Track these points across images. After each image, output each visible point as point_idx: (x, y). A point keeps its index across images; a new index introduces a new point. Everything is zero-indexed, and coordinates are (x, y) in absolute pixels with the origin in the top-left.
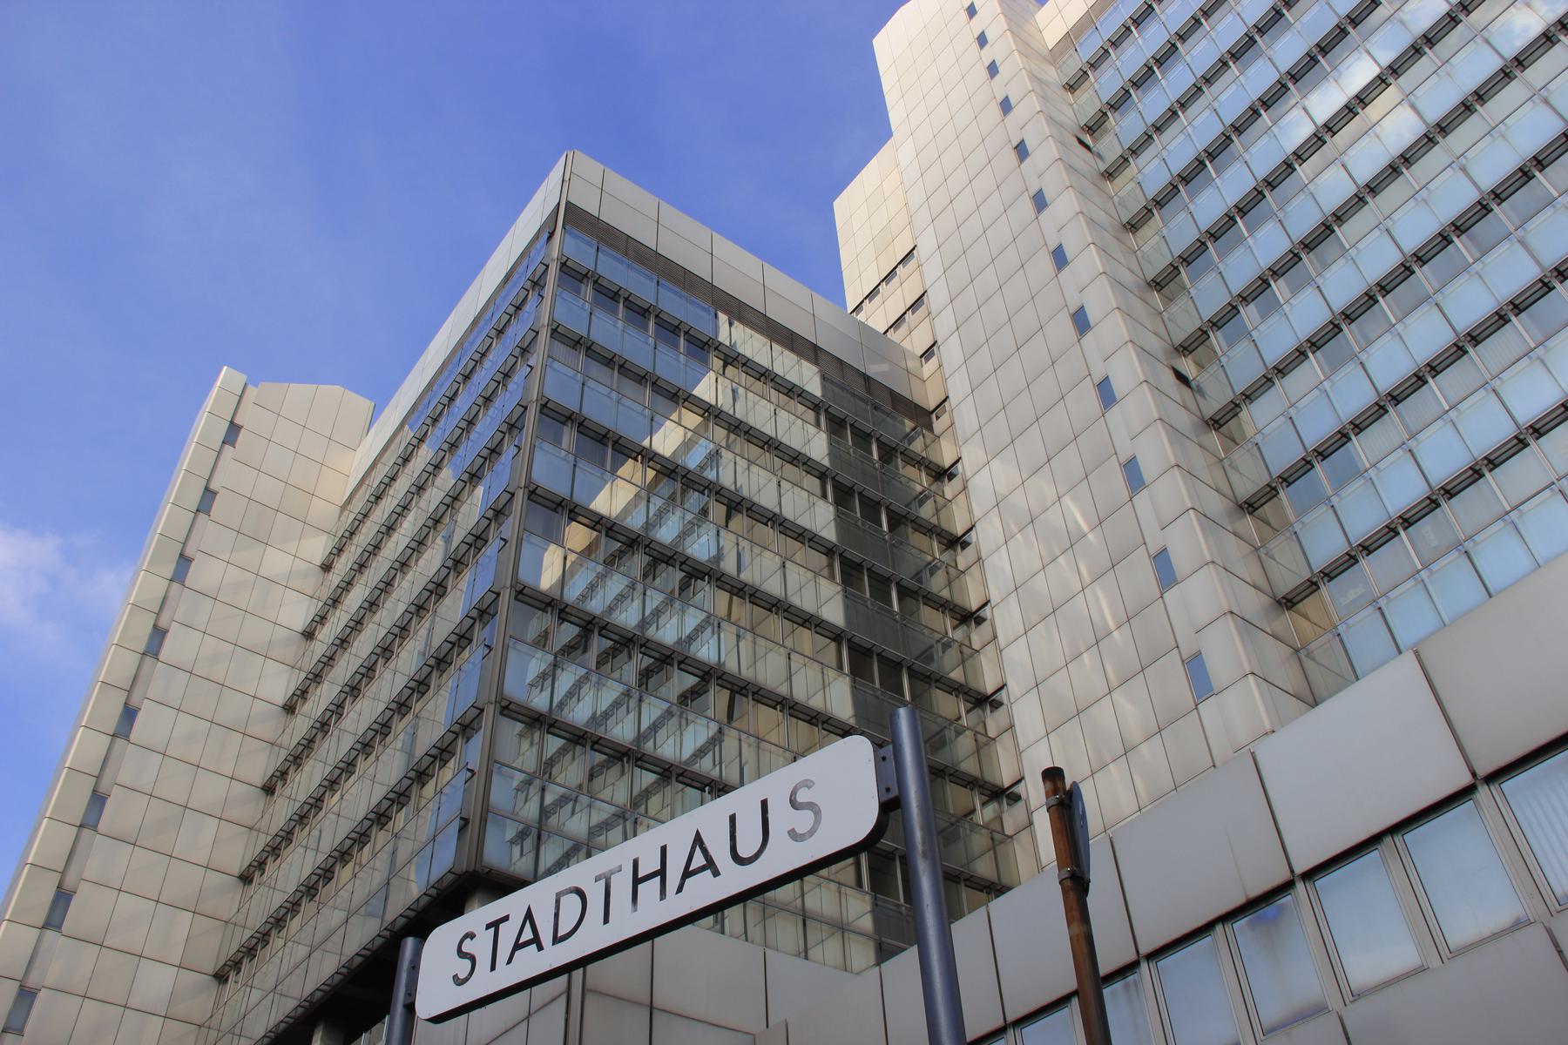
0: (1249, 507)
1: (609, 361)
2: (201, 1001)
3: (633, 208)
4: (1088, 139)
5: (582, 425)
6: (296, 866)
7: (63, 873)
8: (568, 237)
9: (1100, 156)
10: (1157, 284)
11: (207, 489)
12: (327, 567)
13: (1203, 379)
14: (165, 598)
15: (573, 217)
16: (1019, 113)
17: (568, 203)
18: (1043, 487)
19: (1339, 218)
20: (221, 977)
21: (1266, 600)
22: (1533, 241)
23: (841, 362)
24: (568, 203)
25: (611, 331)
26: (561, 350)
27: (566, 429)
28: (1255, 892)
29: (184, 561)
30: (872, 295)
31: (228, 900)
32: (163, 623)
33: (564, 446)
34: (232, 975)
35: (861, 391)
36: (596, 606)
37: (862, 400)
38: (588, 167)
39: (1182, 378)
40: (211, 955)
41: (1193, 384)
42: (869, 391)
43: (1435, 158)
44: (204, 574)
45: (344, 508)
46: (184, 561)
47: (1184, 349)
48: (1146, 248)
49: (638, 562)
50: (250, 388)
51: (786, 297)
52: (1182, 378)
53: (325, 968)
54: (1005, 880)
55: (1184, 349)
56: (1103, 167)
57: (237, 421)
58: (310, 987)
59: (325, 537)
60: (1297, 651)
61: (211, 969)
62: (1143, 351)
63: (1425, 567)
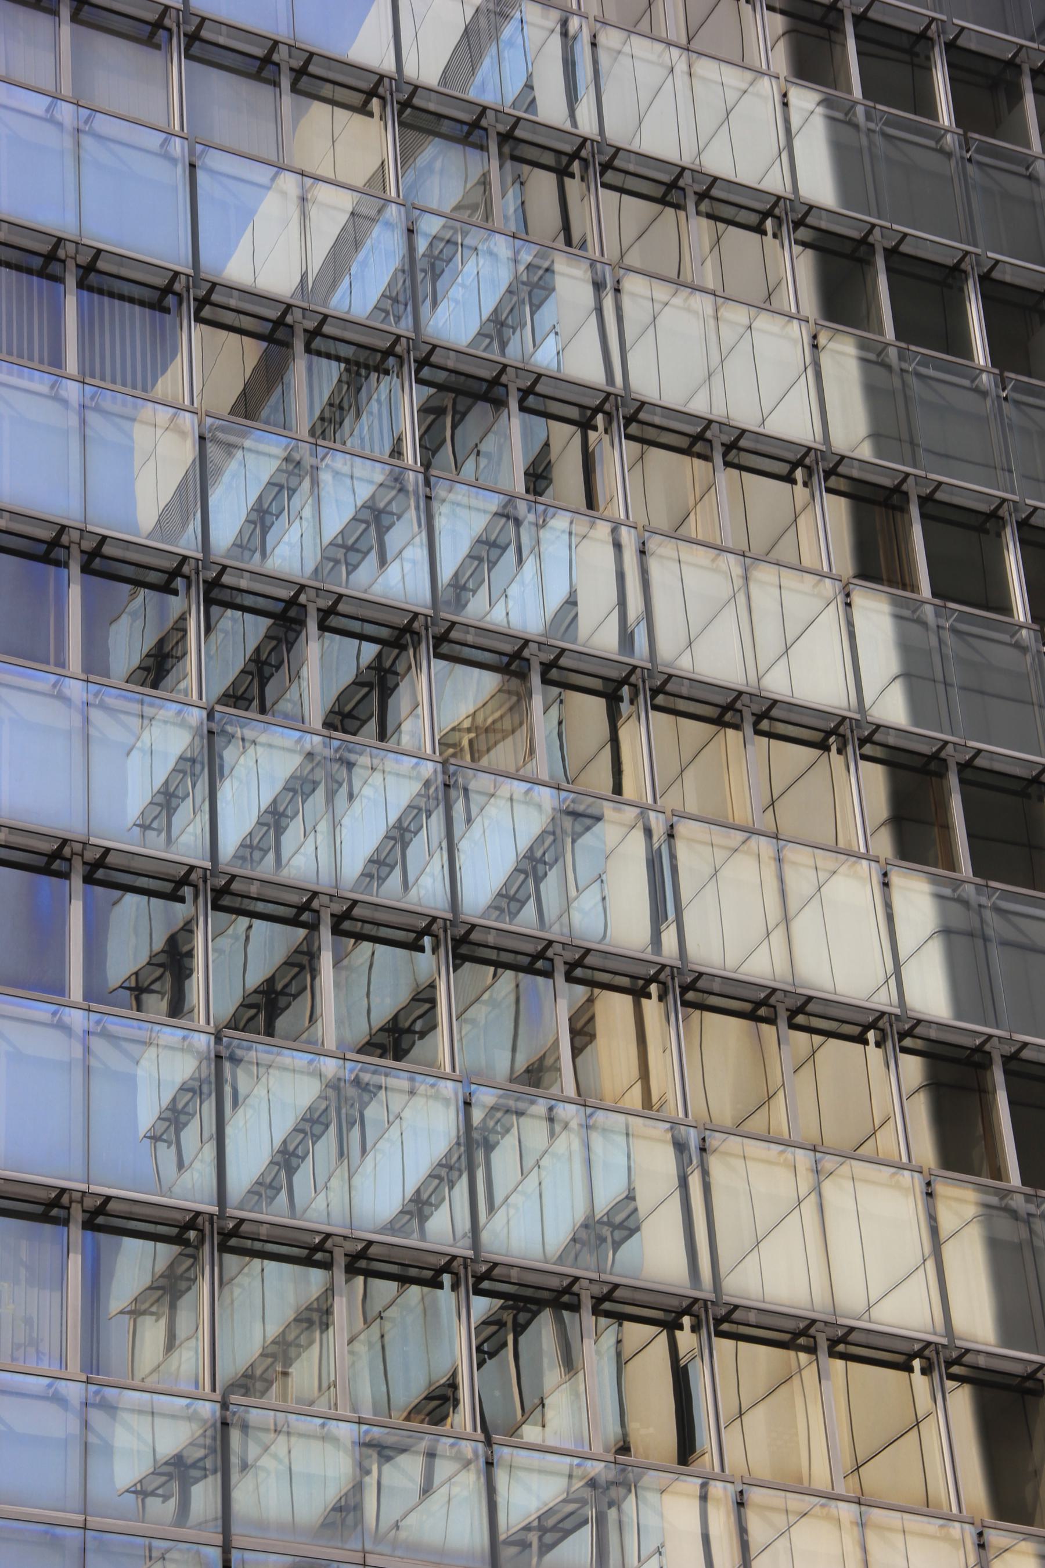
49: (397, 406)
59: (883, 829)
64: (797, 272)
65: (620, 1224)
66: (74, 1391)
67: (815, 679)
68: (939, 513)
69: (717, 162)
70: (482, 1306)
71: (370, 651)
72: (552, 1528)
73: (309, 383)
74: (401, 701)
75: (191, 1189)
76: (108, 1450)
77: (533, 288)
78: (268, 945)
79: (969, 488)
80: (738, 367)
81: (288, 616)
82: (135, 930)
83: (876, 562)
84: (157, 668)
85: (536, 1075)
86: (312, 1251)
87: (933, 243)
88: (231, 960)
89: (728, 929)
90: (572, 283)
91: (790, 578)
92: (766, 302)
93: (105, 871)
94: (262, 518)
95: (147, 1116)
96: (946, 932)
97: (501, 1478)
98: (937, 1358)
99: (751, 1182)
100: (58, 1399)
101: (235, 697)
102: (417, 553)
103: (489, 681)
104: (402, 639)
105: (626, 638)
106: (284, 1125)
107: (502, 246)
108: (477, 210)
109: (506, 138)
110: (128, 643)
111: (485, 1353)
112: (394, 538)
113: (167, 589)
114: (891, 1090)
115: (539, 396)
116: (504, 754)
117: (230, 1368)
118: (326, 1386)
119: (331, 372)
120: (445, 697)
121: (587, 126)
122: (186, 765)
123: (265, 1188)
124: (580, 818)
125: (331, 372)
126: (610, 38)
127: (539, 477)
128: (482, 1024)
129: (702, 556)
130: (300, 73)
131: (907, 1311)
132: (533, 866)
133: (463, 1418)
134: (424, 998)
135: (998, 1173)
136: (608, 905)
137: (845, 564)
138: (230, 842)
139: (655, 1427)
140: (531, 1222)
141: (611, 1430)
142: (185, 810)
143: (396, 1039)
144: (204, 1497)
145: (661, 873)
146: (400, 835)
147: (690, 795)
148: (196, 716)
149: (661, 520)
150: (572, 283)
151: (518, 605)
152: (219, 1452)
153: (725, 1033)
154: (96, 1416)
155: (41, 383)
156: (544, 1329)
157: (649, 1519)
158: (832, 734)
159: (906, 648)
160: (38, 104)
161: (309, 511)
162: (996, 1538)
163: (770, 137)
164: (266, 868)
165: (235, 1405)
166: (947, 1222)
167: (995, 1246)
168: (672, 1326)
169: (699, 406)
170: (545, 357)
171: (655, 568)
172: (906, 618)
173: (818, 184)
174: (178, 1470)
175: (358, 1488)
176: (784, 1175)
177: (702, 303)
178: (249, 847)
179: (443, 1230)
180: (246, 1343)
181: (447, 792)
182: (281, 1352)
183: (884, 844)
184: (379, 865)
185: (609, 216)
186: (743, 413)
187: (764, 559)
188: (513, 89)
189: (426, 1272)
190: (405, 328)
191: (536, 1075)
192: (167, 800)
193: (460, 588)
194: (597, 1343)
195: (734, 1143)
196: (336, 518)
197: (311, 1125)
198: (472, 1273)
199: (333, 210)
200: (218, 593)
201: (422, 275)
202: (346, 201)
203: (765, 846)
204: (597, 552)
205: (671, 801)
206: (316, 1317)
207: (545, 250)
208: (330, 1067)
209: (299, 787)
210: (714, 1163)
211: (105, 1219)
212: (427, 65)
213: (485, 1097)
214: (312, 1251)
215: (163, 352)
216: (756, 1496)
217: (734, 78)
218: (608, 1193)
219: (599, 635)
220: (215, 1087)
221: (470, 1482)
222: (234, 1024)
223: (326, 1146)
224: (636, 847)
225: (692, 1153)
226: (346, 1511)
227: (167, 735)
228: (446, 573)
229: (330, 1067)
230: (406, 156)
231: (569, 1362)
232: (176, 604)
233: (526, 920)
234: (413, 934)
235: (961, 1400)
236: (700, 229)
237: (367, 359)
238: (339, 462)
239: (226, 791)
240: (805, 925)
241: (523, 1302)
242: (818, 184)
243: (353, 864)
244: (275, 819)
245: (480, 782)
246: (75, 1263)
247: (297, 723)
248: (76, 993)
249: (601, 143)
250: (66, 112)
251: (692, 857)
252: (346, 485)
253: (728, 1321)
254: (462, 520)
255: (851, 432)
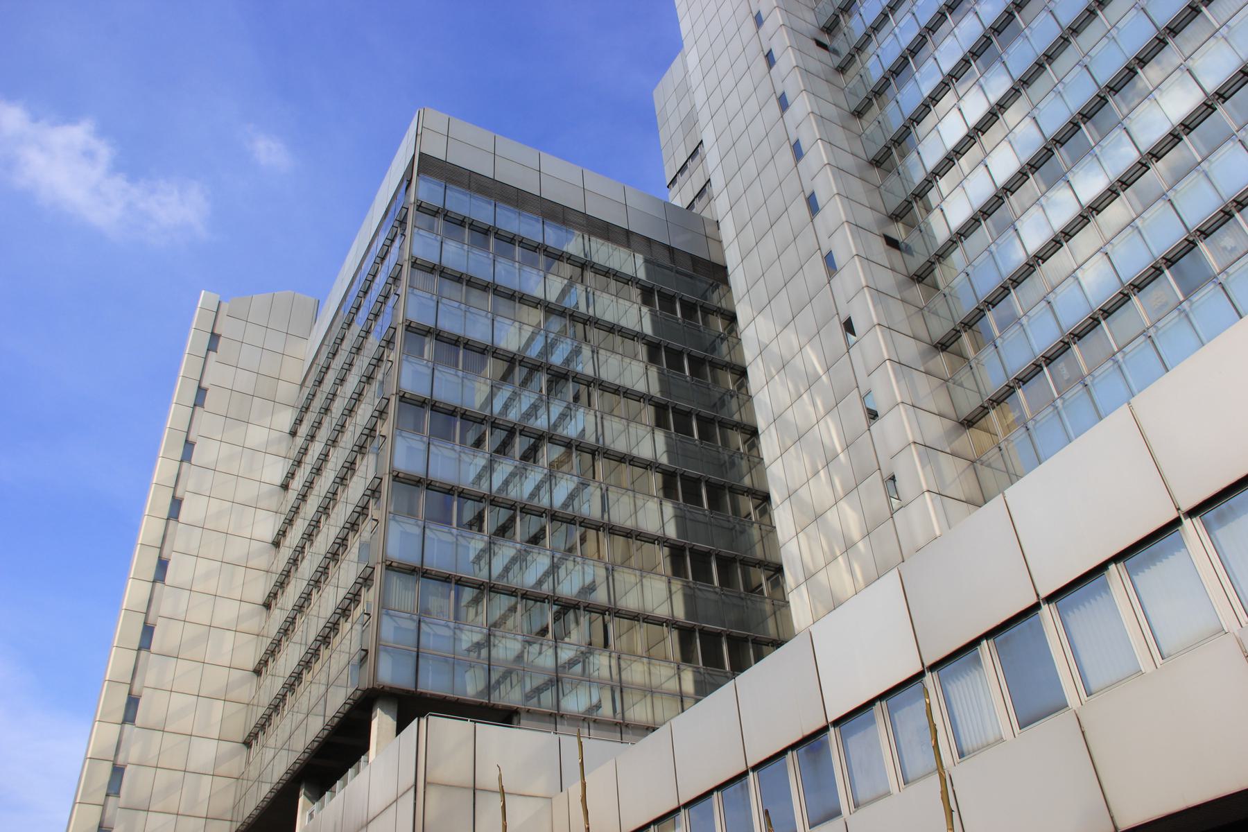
0: (942, 346)
1: (458, 278)
2: (235, 765)
3: (473, 147)
4: (825, 39)
5: (438, 335)
6: (290, 657)
7: (131, 684)
8: (421, 182)
9: (835, 52)
10: (877, 162)
11: (199, 387)
12: (293, 433)
13: (914, 240)
14: (178, 475)
15: (427, 165)
16: (769, 26)
17: (421, 154)
18: (791, 337)
19: (1049, 57)
20: (247, 744)
21: (949, 424)
22: (1134, 129)
23: (648, 240)
24: (421, 154)
25: (456, 254)
26: (420, 275)
27: (427, 339)
28: (807, 732)
29: (189, 445)
30: (683, 169)
31: (246, 690)
32: (179, 494)
33: (426, 357)
34: (254, 742)
35: (667, 262)
36: (513, 415)
37: (667, 268)
38: (436, 119)
39: (892, 243)
40: (240, 729)
41: (903, 246)
42: (673, 260)
43: (1066, 60)
44: (204, 453)
45: (302, 385)
46: (189, 445)
47: (896, 217)
48: (867, 132)
49: (542, 380)
50: (223, 304)
51: (601, 195)
52: (892, 243)
53: (316, 727)
54: (782, 637)
55: (896, 217)
56: (837, 61)
57: (216, 331)
58: (311, 737)
59: (291, 410)
60: (973, 462)
61: (241, 739)
62: (856, 227)
63: (1120, 350)
64: (642, 350)
65: (591, 588)
66: (452, 625)
67: (644, 450)
68: (676, 411)
69: (623, 323)
70: (555, 608)
71: (532, 441)
72: (572, 663)
73: (519, 373)
74: (540, 454)
75: (482, 576)
76: (460, 640)
77: (577, 352)
78: (504, 515)
79: (684, 405)
80: (627, 373)
81: (511, 431)
82: (470, 510)
83: (661, 423)
84: (478, 443)
85: (571, 550)
86: (512, 593)
87: (676, 345)
88: (492, 519)
89: (621, 514)
90: (586, 351)
91: (639, 426)
92: (635, 357)
93: (463, 495)
94: (506, 407)
95: (472, 556)
96: (676, 516)
97: (559, 651)
98: (671, 623)
99: (625, 578)
100: (448, 626)
101: (497, 451)
102: (545, 416)
103: (562, 449)
104: (540, 438)
105: (597, 440)
106: (506, 561)
107: (569, 341)
108: (563, 333)
109: (571, 315)
110: (471, 437)
111: (556, 619)
112: (539, 413)
113: (481, 423)
114: (661, 556)
115: (577, 378)
116: (565, 468)
117: (491, 621)
118: (515, 627)
119: (525, 371)
120: (549, 453)
121: (591, 313)
122: (484, 468)
123: (501, 576)
124: (584, 485)
125: (525, 371)
126: (598, 293)
127: (576, 398)
128: (555, 537)
129: (617, 419)
130: (521, 298)
131: (662, 611)
132: (572, 497)
133: (550, 635)
134: (543, 530)
135: (687, 577)
136: (590, 507)
137: (653, 423)
138: (495, 488)
139: (598, 639)
140: (569, 587)
141: (587, 639)
142: (484, 480)
143: (536, 539)
144: (484, 652)
145: (604, 499)
146: (538, 488)
147: (612, 480)
148: (487, 456)
149: (607, 410)
150: (586, 351)
151: (571, 430)
152: (488, 642)
153: (620, 540)
154: (458, 632)
155: (452, 371)
156: (571, 615)
157: (596, 662)
158: (648, 465)
159: (668, 444)
160: (456, 304)
161: (517, 404)
162: (682, 667)
163: (636, 318)
164: (504, 495)
165: (494, 627)
166: (674, 589)
167: (685, 596)
168: (603, 614)
169: (617, 382)
170: (579, 369)
171: (606, 423)
172: (668, 437)
173: (648, 329)
174: (478, 646)
175: (523, 652)
176: (633, 578)
177: (619, 357)
178: (499, 490)
179: (546, 588)
180: (497, 614)
181: (550, 477)
182: (504, 618)
183: (661, 494)
184: (533, 495)
185: (595, 334)
186: (628, 385)
187: (634, 420)
188: (573, 303)
189: (541, 599)
190: (544, 360)
191: (571, 550)
192: (479, 477)
193: (555, 426)
194: (584, 619)
195: (621, 569)
196: (525, 407)
197: (513, 560)
198: (554, 600)
199: (527, 331)
200: (494, 425)
201: (549, 348)
202: (531, 329)
203: (631, 493)
204: (591, 418)
205: (607, 481)
206: (513, 609)
207: (580, 343)
208: (518, 546)
209: (513, 475)
210: (616, 575)
211: (460, 582)
212: (552, 297)
213: (558, 555)
214: (512, 593)
215: (484, 365)
216: (623, 656)
217: (628, 303)
218: (588, 580)
219: (590, 438)
220: (489, 550)
221: (550, 652)
222: (495, 534)
223: (517, 566)
224: (598, 493)
225: (610, 571)
226: (520, 657)
227: (481, 461)
228: (552, 421)
229: (518, 546)
230: (546, 319)
231: (577, 623)
232: (483, 427)
233: (569, 511)
234: (540, 513)
235: (675, 633)
236: (618, 339)
237: (534, 368)
238: (526, 393)
239: (495, 476)
240: (640, 514)
241: (566, 608)
242: (648, 329)
243: (526, 494)
244: (506, 483)
245: (560, 475)
246: (453, 593)
247: (513, 458)
248: (455, 524)
249: (594, 317)
250: (463, 306)
251: (612, 496)
252: (527, 400)
253: (618, 613)
254: (557, 409)
255: (655, 390)
